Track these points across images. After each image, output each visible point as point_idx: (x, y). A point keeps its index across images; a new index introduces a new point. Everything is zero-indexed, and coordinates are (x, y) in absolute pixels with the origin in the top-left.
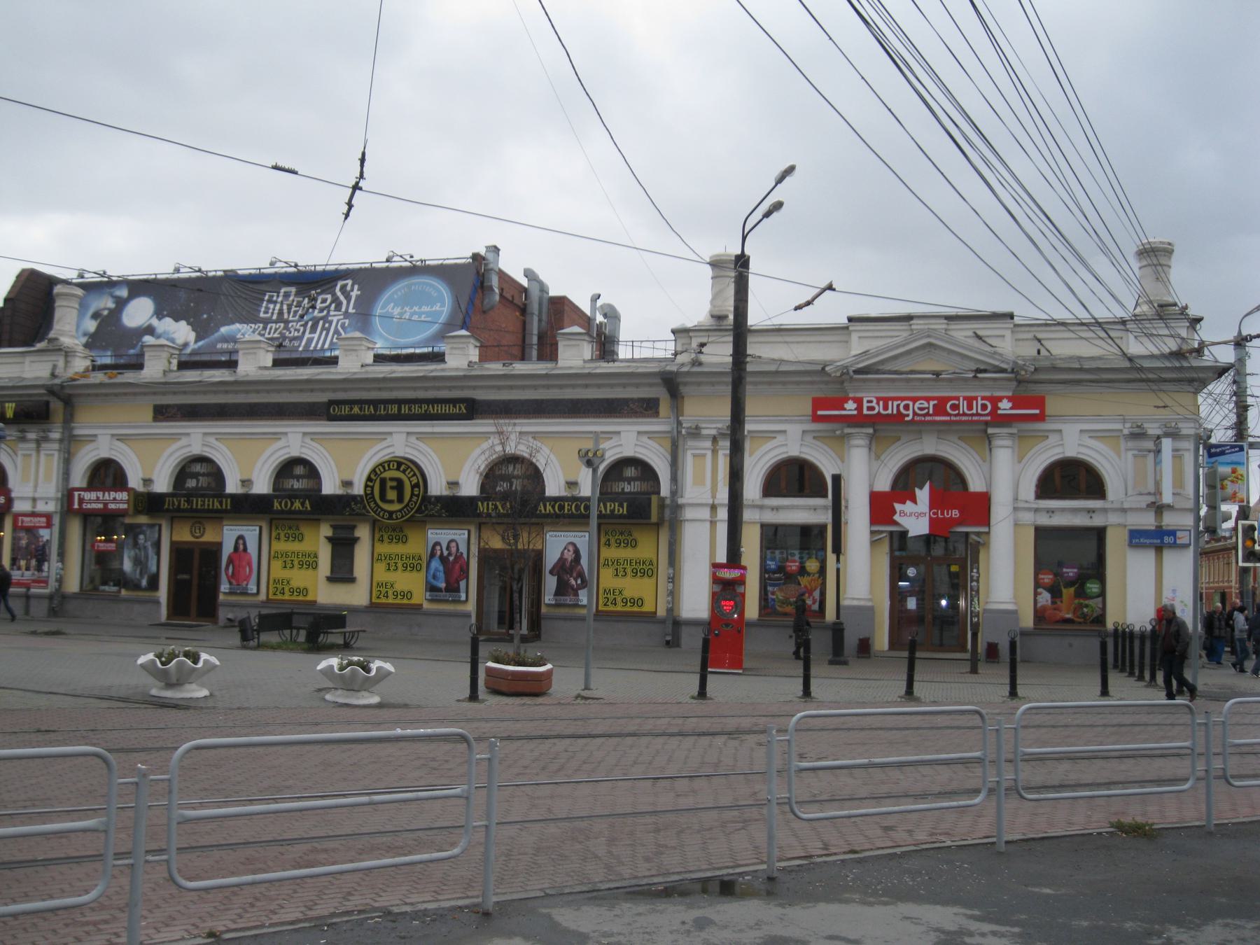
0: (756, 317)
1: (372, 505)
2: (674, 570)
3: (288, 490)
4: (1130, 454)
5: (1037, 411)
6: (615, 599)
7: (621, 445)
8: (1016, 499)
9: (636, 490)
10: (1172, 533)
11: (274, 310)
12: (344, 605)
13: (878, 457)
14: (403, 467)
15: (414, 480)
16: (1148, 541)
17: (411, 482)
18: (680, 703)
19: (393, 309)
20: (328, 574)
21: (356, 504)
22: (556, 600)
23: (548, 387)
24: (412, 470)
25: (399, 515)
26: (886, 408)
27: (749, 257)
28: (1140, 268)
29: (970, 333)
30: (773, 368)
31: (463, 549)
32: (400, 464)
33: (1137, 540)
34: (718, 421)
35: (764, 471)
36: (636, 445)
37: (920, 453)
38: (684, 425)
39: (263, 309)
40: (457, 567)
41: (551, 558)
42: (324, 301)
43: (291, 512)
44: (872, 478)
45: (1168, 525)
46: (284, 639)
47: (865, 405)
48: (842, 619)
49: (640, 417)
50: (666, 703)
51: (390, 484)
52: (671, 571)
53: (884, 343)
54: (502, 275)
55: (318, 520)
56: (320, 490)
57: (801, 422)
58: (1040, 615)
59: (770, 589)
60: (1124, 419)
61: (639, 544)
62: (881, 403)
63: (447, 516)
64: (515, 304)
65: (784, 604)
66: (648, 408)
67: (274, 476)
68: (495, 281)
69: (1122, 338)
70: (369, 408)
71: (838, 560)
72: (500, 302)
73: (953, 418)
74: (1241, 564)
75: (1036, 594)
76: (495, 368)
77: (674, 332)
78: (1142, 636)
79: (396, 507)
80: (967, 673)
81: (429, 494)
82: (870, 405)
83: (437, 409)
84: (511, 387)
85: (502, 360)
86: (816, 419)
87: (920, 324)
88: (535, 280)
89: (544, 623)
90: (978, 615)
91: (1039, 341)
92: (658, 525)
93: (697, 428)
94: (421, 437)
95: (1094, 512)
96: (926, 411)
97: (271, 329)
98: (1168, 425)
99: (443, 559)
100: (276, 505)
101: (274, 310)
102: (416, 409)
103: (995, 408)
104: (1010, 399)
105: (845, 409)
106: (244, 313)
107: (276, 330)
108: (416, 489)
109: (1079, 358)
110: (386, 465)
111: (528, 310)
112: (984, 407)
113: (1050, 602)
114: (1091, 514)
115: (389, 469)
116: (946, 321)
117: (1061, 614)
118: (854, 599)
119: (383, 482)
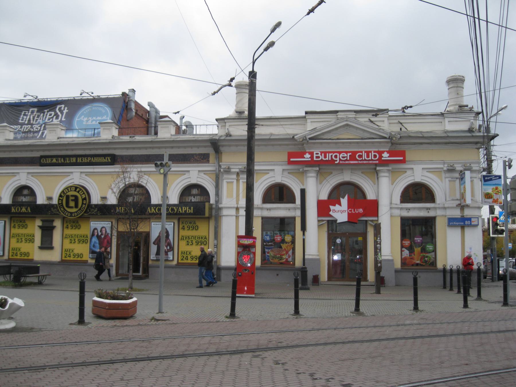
0: (259, 113)
1: (62, 209)
2: (217, 241)
3: (20, 202)
4: (447, 180)
5: (402, 158)
6: (187, 257)
7: (190, 178)
8: (391, 203)
9: (198, 201)
10: (470, 219)
11: (26, 119)
12: (52, 261)
13: (321, 183)
14: (78, 190)
15: (84, 196)
16: (457, 223)
17: (82, 197)
18: (218, 322)
19: (83, 118)
20: (40, 245)
21: (54, 209)
22: (157, 257)
23: (153, 148)
24: (83, 191)
25: (76, 214)
26: (325, 157)
27: (256, 72)
28: (449, 89)
29: (367, 120)
30: (268, 137)
31: (109, 231)
32: (76, 188)
33: (452, 223)
34: (240, 165)
35: (262, 192)
36: (197, 177)
37: (331, 187)
38: (222, 167)
39: (21, 119)
40: (106, 240)
41: (154, 236)
42: (50, 115)
43: (20, 213)
44: (318, 193)
45: (467, 215)
46: (6, 280)
47: (315, 155)
48: (306, 266)
49: (199, 163)
50: (210, 322)
51: (71, 198)
52: (216, 242)
53: (323, 124)
54: (136, 103)
55: (35, 217)
56: (36, 202)
57: (282, 165)
58: (404, 262)
59: (266, 250)
60: (444, 163)
61: (200, 229)
62: (323, 154)
63: (101, 215)
64: (143, 118)
65: (274, 258)
66: (204, 158)
67: (13, 194)
68: (133, 106)
69: (442, 122)
70: (61, 160)
71: (304, 234)
72: (135, 116)
73: (359, 162)
74: (491, 235)
75: (402, 251)
76: (126, 138)
77: (217, 120)
78: (458, 271)
79: (74, 210)
80: (373, 293)
81: (92, 203)
82: (317, 155)
83: (96, 160)
84: (134, 148)
85: (130, 135)
86: (290, 163)
87: (343, 115)
88: (153, 107)
89: (150, 270)
90: (381, 262)
91: (401, 123)
92: (209, 218)
93: (229, 168)
94: (88, 174)
95: (430, 209)
96: (346, 158)
97: (24, 128)
98: (465, 166)
99: (98, 237)
100: (13, 210)
101: (26, 119)
102: (85, 160)
103: (381, 157)
104: (388, 152)
105: (304, 158)
106: (12, 120)
107: (27, 128)
108: (85, 201)
109: (421, 132)
110: (69, 189)
111: (150, 121)
112: (375, 156)
113: (408, 255)
114: (428, 210)
115: (71, 191)
116: (355, 114)
117: (414, 261)
118: (310, 255)
119: (68, 197)
